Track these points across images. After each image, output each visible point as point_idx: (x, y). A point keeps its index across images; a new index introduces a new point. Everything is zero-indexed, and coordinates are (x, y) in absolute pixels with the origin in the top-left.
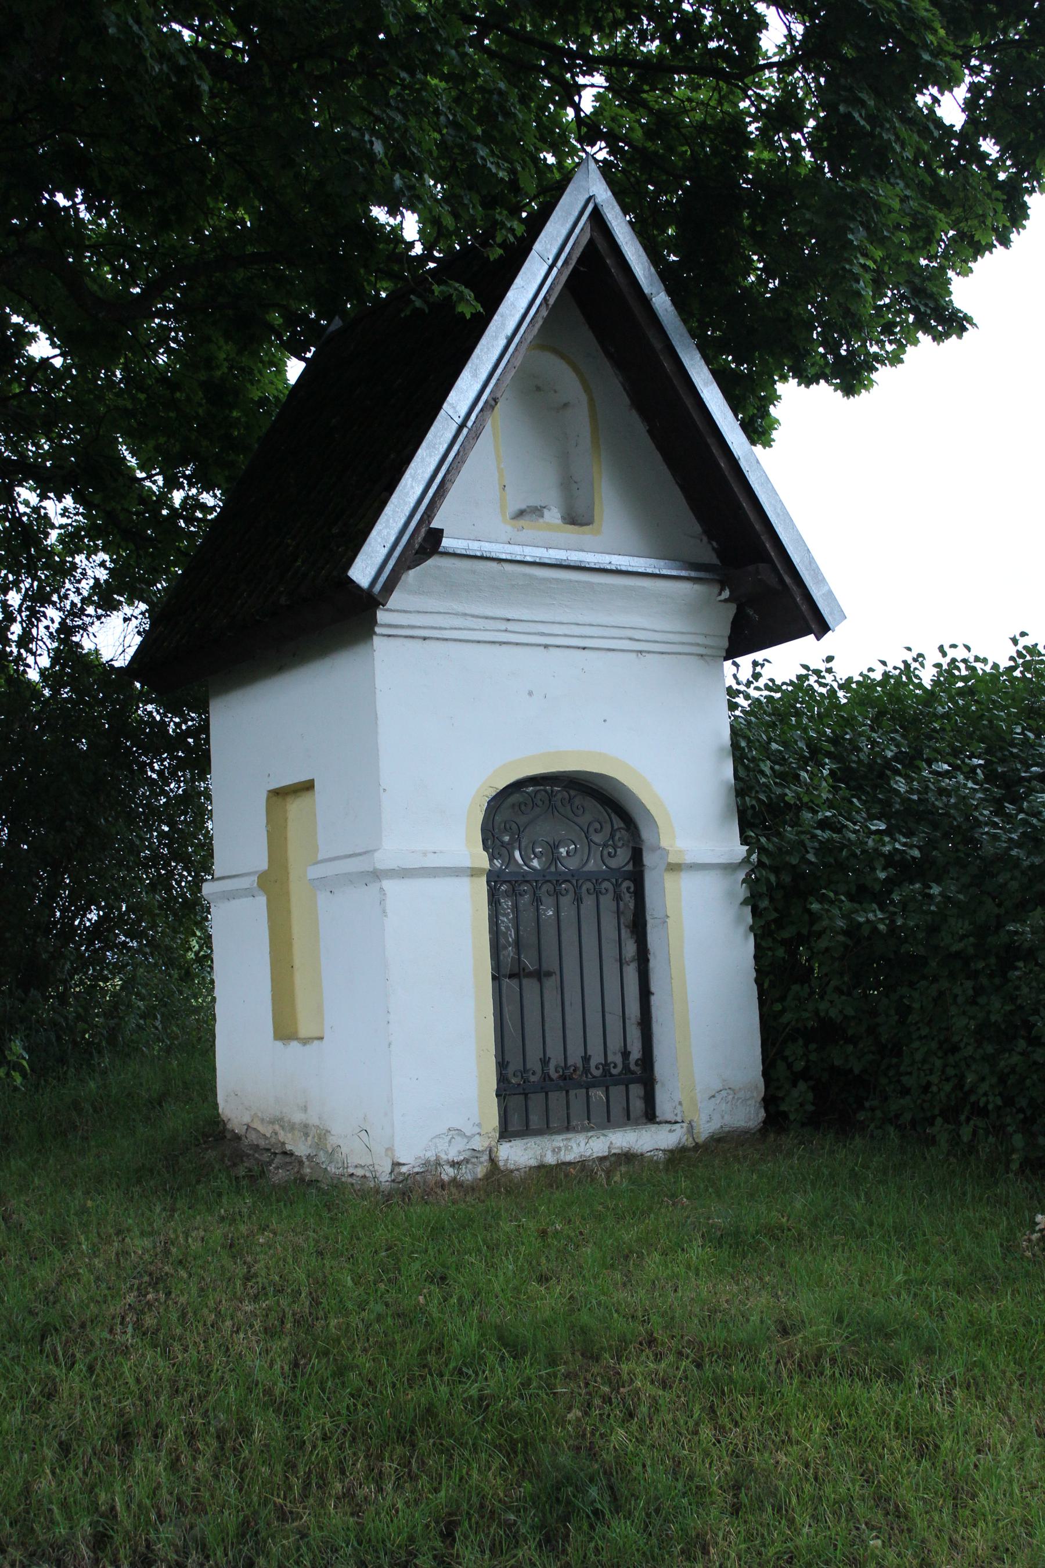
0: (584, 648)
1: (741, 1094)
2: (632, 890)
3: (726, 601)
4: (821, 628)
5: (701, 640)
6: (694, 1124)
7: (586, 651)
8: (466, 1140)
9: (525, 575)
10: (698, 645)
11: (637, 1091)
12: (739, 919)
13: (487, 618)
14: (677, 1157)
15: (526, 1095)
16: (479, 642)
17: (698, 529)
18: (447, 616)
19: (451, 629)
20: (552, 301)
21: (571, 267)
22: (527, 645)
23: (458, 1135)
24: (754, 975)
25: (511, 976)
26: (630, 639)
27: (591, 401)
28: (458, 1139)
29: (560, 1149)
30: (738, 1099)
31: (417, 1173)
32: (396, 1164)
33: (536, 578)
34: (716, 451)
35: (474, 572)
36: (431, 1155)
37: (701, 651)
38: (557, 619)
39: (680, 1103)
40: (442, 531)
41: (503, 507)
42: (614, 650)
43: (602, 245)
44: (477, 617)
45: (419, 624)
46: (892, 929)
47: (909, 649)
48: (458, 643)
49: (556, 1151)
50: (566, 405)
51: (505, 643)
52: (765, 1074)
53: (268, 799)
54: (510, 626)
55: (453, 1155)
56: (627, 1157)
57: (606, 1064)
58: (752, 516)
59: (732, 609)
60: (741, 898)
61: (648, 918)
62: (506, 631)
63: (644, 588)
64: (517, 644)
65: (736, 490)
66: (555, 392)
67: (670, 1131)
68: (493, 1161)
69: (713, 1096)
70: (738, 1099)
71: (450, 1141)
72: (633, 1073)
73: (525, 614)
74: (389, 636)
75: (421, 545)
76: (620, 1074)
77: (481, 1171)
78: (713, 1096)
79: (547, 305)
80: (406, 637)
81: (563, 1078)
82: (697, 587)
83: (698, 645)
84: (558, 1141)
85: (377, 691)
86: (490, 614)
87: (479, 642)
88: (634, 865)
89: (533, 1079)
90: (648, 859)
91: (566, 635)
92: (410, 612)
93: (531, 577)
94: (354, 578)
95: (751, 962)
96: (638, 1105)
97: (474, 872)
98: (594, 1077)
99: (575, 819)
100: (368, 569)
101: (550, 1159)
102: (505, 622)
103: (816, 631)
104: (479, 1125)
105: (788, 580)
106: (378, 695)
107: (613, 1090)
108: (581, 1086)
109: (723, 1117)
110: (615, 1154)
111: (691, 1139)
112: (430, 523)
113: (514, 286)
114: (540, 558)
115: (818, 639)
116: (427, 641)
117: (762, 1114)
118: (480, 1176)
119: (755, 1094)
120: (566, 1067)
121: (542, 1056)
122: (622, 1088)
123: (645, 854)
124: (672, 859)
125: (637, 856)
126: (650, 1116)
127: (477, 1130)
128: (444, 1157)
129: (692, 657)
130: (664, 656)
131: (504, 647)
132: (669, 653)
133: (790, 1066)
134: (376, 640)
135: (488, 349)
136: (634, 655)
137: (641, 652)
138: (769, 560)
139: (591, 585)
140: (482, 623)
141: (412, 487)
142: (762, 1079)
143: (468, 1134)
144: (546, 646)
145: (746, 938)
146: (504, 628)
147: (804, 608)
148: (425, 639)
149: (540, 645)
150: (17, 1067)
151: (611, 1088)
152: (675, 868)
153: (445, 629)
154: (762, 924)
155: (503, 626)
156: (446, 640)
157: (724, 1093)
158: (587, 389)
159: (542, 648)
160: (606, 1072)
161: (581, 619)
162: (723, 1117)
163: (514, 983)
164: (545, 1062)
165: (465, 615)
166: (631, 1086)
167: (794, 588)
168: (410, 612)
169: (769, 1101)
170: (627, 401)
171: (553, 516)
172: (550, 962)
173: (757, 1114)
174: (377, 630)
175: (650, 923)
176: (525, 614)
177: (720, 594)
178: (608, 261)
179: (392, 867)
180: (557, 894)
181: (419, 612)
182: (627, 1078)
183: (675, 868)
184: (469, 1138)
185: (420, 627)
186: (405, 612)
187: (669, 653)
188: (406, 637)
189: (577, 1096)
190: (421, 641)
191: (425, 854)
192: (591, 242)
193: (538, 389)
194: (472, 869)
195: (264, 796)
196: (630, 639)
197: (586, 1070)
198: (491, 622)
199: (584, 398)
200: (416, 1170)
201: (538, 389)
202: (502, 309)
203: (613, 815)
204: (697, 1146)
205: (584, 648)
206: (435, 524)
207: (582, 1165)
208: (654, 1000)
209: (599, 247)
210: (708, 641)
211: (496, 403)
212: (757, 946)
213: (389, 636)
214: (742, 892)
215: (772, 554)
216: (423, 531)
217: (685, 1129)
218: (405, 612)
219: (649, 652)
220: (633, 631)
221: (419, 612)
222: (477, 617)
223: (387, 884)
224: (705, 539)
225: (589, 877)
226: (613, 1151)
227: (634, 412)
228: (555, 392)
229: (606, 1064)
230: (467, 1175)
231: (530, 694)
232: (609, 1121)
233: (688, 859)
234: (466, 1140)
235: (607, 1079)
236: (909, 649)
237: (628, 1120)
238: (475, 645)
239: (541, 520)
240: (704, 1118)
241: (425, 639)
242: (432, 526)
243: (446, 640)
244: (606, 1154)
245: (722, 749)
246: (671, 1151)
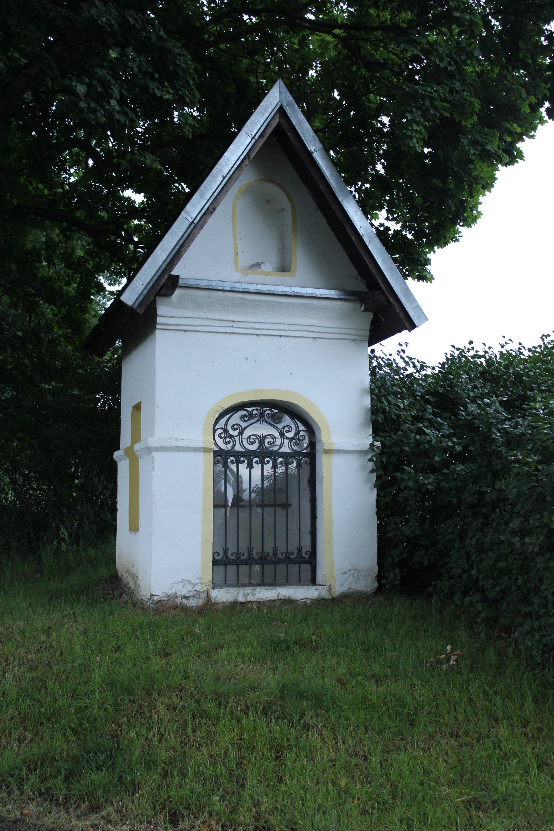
0: (281, 336)
1: (363, 573)
2: (308, 462)
3: (364, 311)
4: (412, 326)
5: (352, 332)
6: (332, 587)
7: (281, 338)
8: (192, 586)
9: (240, 298)
10: (351, 334)
11: (306, 568)
12: (368, 480)
13: (221, 320)
14: (319, 602)
15: (238, 566)
16: (217, 333)
17: (356, 273)
18: (197, 319)
19: (200, 326)
20: (252, 156)
21: (265, 138)
22: (246, 334)
23: (188, 583)
24: (376, 510)
25: (258, 506)
26: (308, 331)
27: (293, 207)
28: (188, 585)
29: (248, 594)
30: (361, 575)
31: (164, 600)
32: (152, 595)
33: (246, 300)
34: (349, 231)
35: (210, 297)
36: (171, 592)
37: (354, 338)
38: (263, 321)
39: (324, 576)
40: (178, 276)
41: (236, 264)
42: (298, 337)
43: (285, 126)
44: (215, 320)
45: (180, 324)
46: (438, 488)
47: (504, 337)
48: (205, 333)
49: (245, 595)
50: (283, 209)
51: (232, 333)
52: (379, 563)
53: (133, 410)
54: (235, 324)
55: (184, 592)
56: (289, 601)
57: (238, 553)
58: (370, 265)
59: (370, 316)
60: (370, 469)
61: (317, 478)
62: (233, 327)
63: (313, 304)
64: (240, 334)
65: (361, 252)
66: (278, 203)
67: (316, 589)
68: (208, 597)
69: (346, 573)
70: (361, 575)
71: (183, 586)
72: (304, 558)
73: (243, 318)
74: (165, 329)
75: (164, 284)
76: (296, 558)
77: (201, 602)
78: (346, 573)
79: (249, 158)
80: (175, 330)
81: (261, 558)
82: (347, 304)
83: (351, 334)
84: (248, 590)
85: (156, 357)
86: (222, 318)
87: (217, 333)
88: (311, 449)
89: (242, 557)
90: (318, 447)
91: (268, 329)
92: (176, 317)
93: (244, 299)
94: (124, 301)
95: (374, 503)
96: (309, 576)
97: (206, 450)
98: (280, 559)
99: (276, 425)
100: (133, 296)
101: (241, 599)
102: (232, 323)
103: (408, 327)
104: (201, 579)
105: (391, 300)
106: (157, 358)
107: (241, 567)
108: (271, 563)
109: (350, 585)
110: (280, 599)
111: (329, 595)
112: (170, 272)
113: (229, 150)
114: (248, 289)
115: (409, 332)
116: (187, 332)
117: (376, 584)
118: (200, 604)
119: (372, 574)
120: (263, 553)
121: (224, 546)
122: (297, 565)
123: (317, 445)
124: (326, 447)
125: (312, 444)
126: (313, 581)
127: (199, 581)
128: (179, 593)
129: (348, 341)
130: (330, 340)
131: (232, 335)
132: (333, 339)
133: (393, 559)
134: (157, 332)
135: (211, 183)
136: (311, 339)
137: (315, 338)
138: (380, 289)
139: (281, 303)
140: (218, 323)
141: (161, 255)
142: (377, 566)
143: (194, 583)
144: (257, 335)
145: (372, 490)
146: (231, 325)
147: (401, 315)
148: (185, 331)
149: (253, 334)
150: (64, 540)
151: (289, 565)
152: (329, 452)
153: (197, 326)
154: (380, 483)
155: (231, 324)
156: (198, 331)
157: (352, 572)
158: (291, 200)
159: (255, 336)
160: (238, 558)
161: (277, 321)
162: (350, 585)
163: (259, 510)
164: (250, 549)
165: (208, 319)
166: (302, 565)
167: (395, 304)
168: (176, 317)
169: (379, 577)
170: (315, 206)
171: (268, 267)
172: (294, 502)
173: (373, 584)
174: (158, 326)
175: (318, 480)
176: (243, 318)
177: (361, 308)
178: (288, 134)
179: (157, 446)
180: (262, 463)
181: (181, 317)
182: (300, 560)
183: (329, 452)
184: (195, 585)
185: (182, 325)
186: (174, 317)
187: (333, 339)
188: (175, 330)
189: (281, 568)
190: (183, 332)
191: (176, 440)
192: (279, 125)
193: (268, 201)
194: (204, 448)
195: (131, 409)
196: (308, 331)
197: (275, 555)
198: (224, 322)
199: (290, 205)
200: (164, 599)
201: (268, 201)
202: (221, 162)
203: (298, 422)
204: (333, 599)
205: (281, 336)
206: (174, 272)
207: (260, 604)
208: (318, 520)
209: (284, 127)
210: (357, 332)
211: (214, 210)
212: (378, 495)
213: (230, 333)
214: (371, 465)
215: (382, 286)
216: (166, 276)
217: (325, 589)
218: (174, 317)
219: (320, 338)
220: (309, 327)
221: (181, 317)
222: (215, 320)
223: (155, 454)
224: (360, 278)
225: (282, 455)
226: (280, 598)
227: (319, 212)
228: (278, 203)
229: (238, 553)
230: (192, 603)
231: (247, 359)
232: (300, 582)
233: (336, 447)
234: (192, 586)
235: (288, 560)
236: (504, 337)
237: (299, 582)
238: (214, 334)
239: (259, 270)
240: (338, 584)
241: (185, 331)
242: (172, 273)
243: (198, 331)
244: (276, 598)
245: (364, 390)
246: (314, 600)
